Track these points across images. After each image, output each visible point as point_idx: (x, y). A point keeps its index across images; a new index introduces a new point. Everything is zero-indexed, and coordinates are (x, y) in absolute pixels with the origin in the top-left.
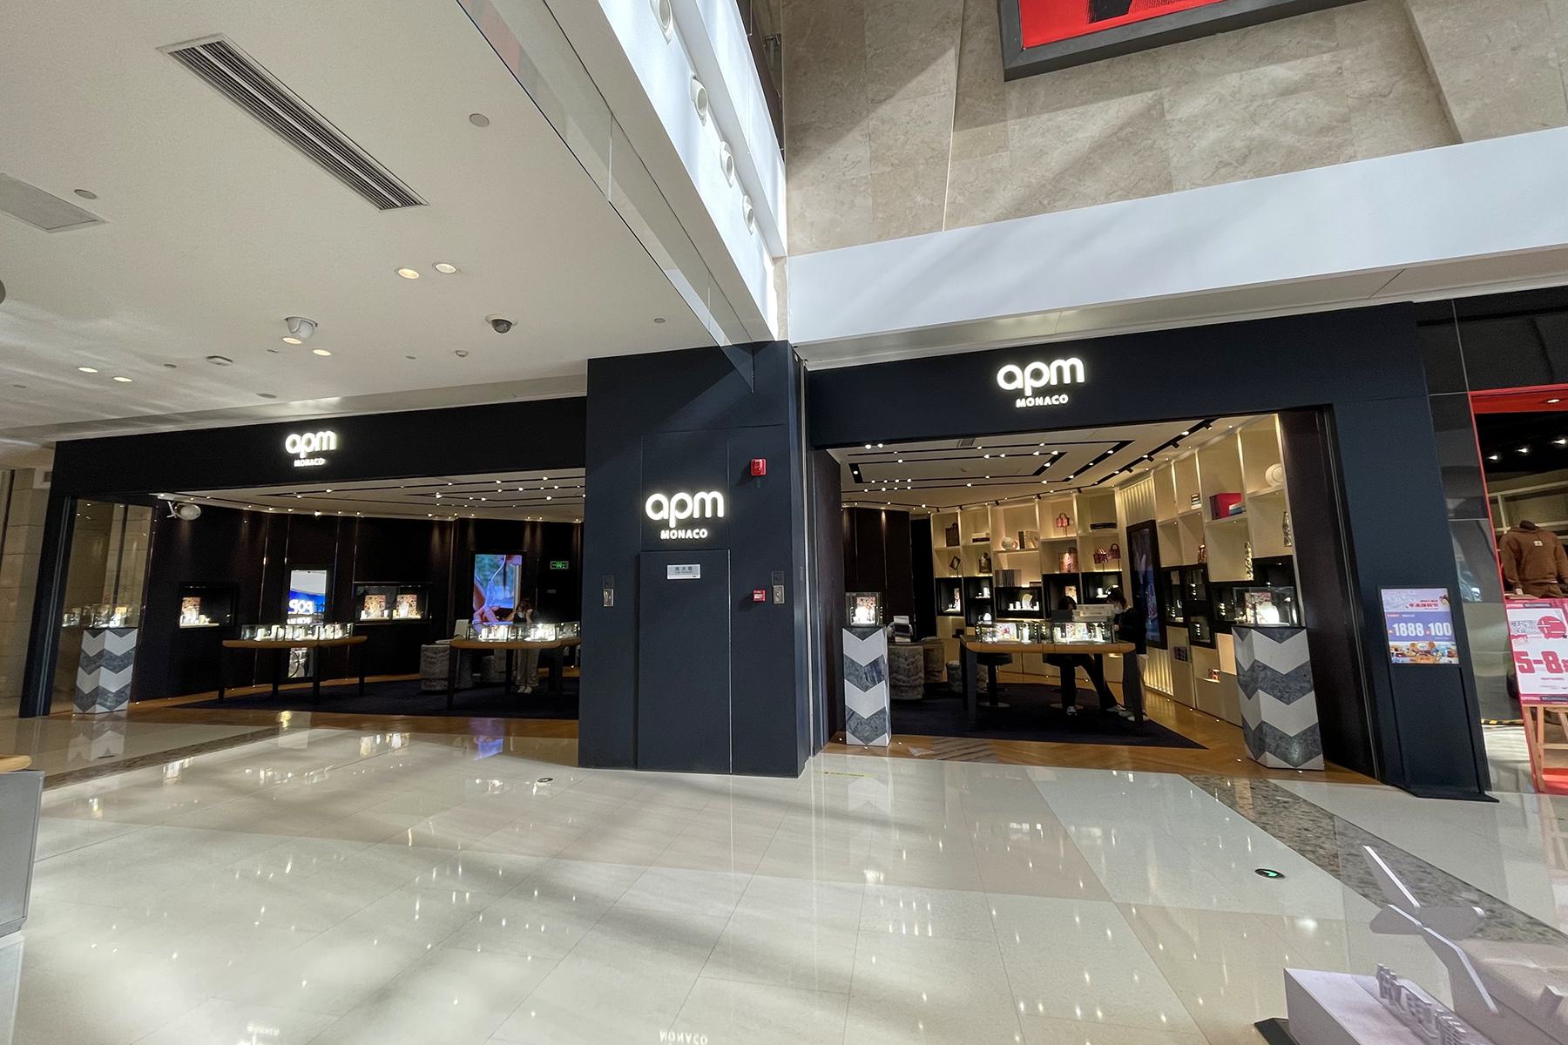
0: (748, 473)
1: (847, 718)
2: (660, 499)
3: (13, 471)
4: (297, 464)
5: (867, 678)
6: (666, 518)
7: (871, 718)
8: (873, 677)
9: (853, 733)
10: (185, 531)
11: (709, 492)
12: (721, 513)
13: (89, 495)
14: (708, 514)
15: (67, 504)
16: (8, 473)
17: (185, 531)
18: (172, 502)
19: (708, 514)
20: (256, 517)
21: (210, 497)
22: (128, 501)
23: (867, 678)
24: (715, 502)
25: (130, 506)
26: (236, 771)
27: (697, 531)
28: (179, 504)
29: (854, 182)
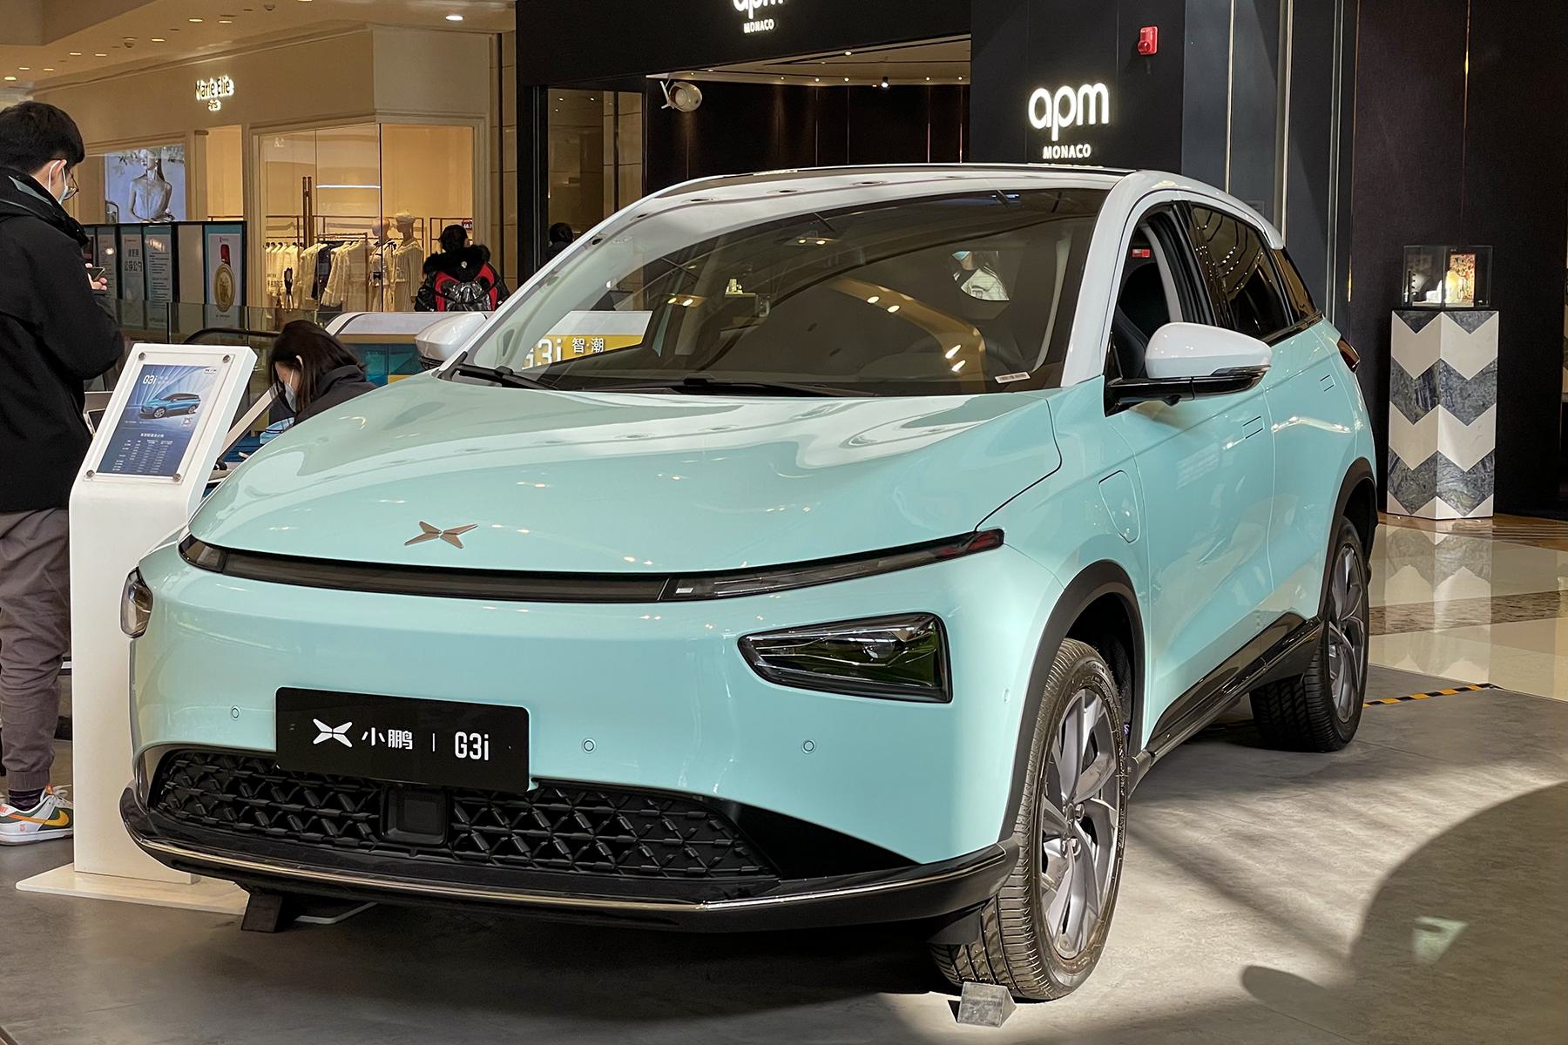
0: (1137, 56)
1: (1389, 468)
2: (1043, 96)
3: (500, 35)
4: (748, 28)
5: (1417, 399)
6: (1049, 126)
7: (1418, 470)
8: (1426, 399)
9: (1395, 494)
10: (688, 130)
11: (1093, 85)
12: (1105, 120)
13: (567, 81)
14: (1092, 121)
15: (536, 93)
16: (495, 38)
17: (688, 130)
18: (665, 81)
19: (1092, 121)
20: (795, 95)
21: (711, 75)
22: (616, 88)
23: (1417, 399)
24: (1099, 97)
25: (619, 93)
26: (1457, 771)
27: (1080, 146)
28: (676, 84)
29: (134, 156)
